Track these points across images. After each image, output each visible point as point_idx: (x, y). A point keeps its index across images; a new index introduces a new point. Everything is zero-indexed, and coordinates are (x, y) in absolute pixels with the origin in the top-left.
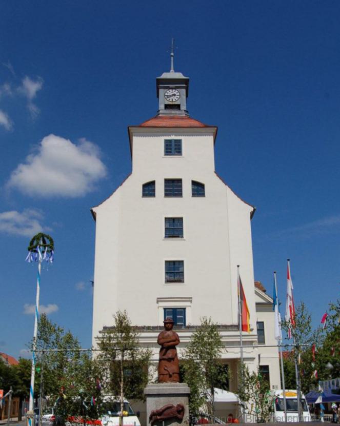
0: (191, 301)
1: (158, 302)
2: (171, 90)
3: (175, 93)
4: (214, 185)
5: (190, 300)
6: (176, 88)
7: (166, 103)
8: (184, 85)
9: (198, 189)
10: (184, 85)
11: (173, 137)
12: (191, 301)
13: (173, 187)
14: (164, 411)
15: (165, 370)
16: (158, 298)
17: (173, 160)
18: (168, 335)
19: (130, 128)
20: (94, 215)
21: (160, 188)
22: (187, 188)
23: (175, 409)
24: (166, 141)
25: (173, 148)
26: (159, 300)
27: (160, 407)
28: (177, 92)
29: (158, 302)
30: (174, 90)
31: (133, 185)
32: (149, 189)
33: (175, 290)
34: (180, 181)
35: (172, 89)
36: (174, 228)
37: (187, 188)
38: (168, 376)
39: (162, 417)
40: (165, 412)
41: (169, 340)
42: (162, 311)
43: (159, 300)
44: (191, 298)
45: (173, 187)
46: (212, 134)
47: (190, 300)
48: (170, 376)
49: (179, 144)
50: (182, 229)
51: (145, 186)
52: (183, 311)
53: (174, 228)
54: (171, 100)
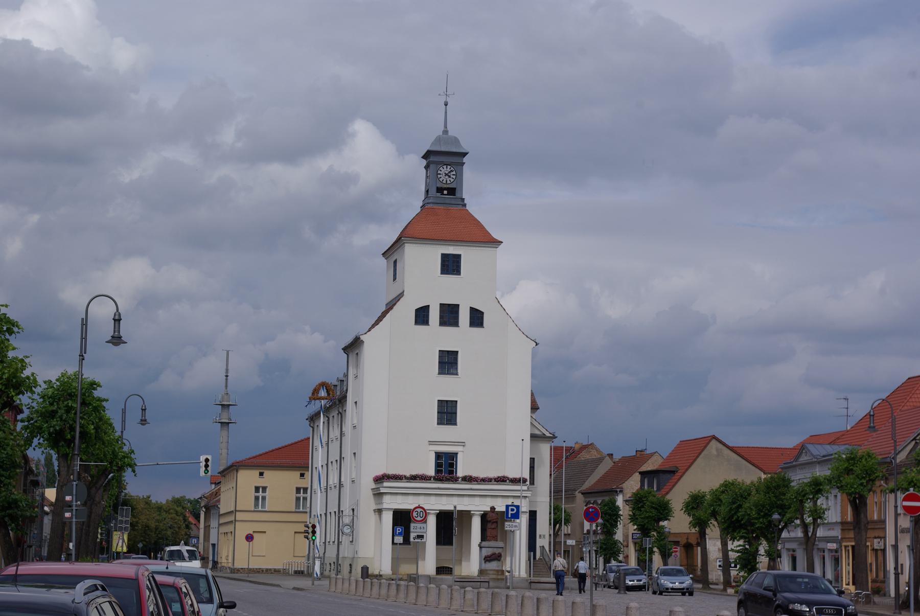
5: (463, 444)
9: (477, 318)
13: (449, 314)
21: (434, 315)
22: (464, 316)
24: (444, 256)
26: (431, 443)
31: (405, 311)
32: (422, 316)
33: (447, 432)
36: (448, 362)
37: (464, 316)
43: (431, 443)
47: (463, 444)
51: (418, 311)
52: (453, 456)
53: (448, 362)
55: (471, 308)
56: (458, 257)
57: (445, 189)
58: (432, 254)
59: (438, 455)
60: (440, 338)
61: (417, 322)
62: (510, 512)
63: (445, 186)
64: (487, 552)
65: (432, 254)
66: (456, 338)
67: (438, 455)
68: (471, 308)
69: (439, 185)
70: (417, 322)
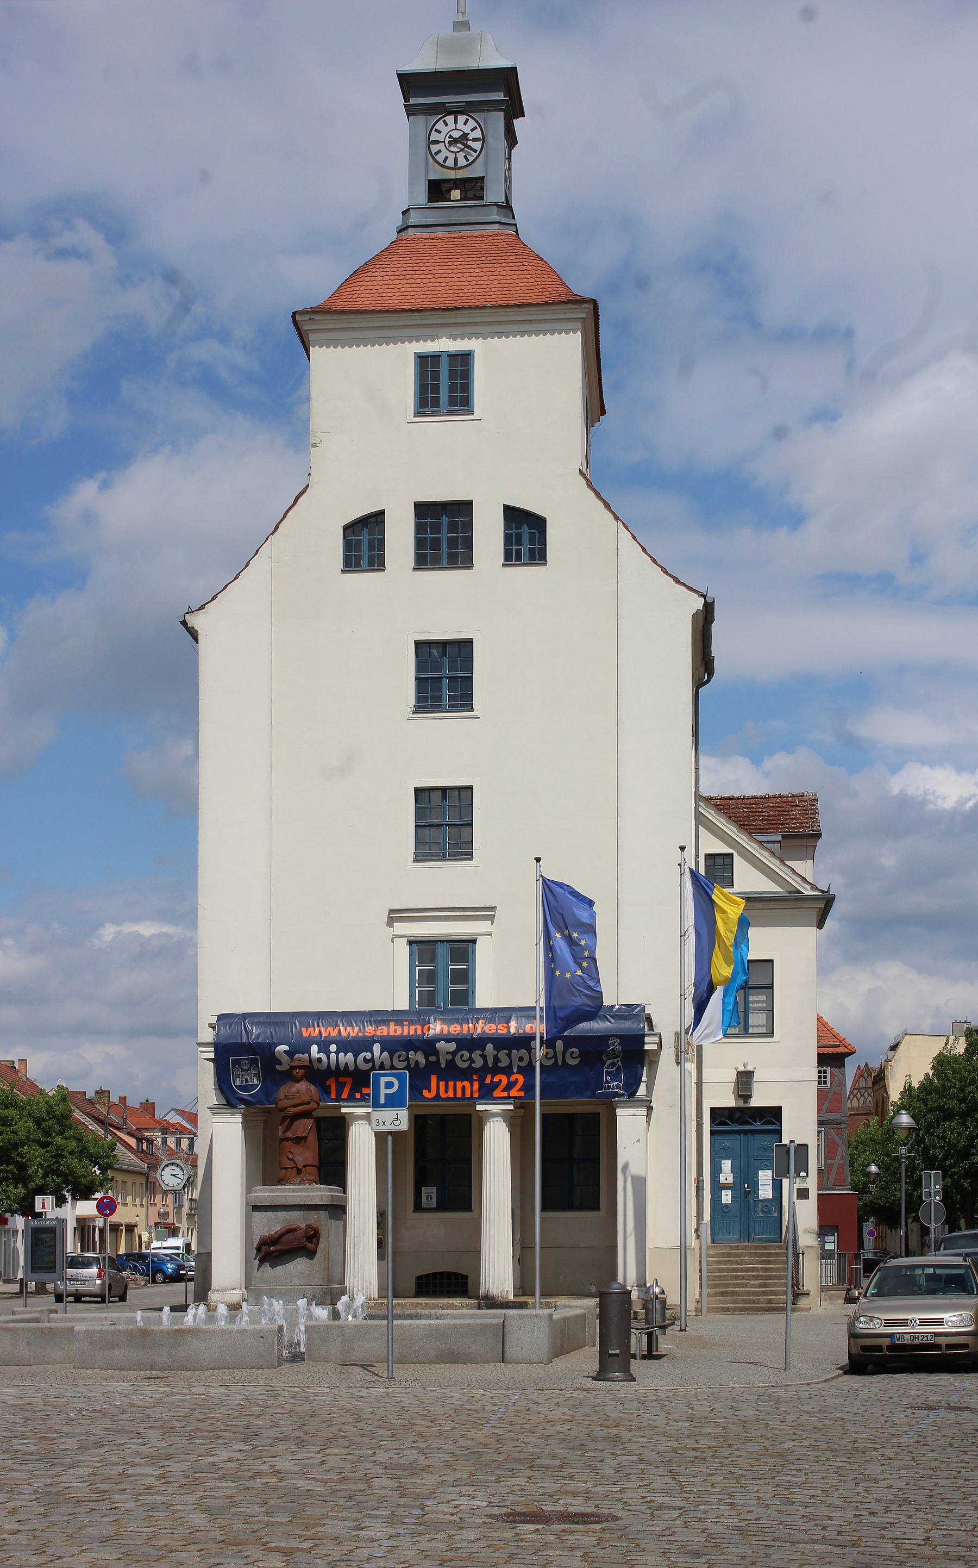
0: (492, 918)
1: (391, 921)
2: (450, 119)
3: (467, 129)
4: (574, 519)
5: (487, 913)
6: (468, 109)
7: (432, 177)
8: (500, 96)
9: (526, 535)
10: (500, 96)
11: (445, 345)
12: (492, 918)
13: (444, 532)
14: (281, 1236)
15: (290, 1159)
16: (392, 911)
17: (444, 429)
18: (298, 1092)
19: (298, 318)
20: (194, 635)
21: (400, 537)
22: (488, 533)
23: (300, 1234)
24: (426, 362)
25: (444, 388)
26: (395, 916)
27: (276, 1229)
28: (472, 124)
29: (391, 921)
30: (462, 118)
32: (363, 542)
33: (444, 882)
34: (464, 508)
35: (456, 112)
36: (444, 675)
37: (488, 533)
38: (295, 1171)
39: (278, 1247)
40: (284, 1239)
41: (297, 1101)
42: (403, 951)
43: (395, 916)
44: (493, 908)
45: (444, 532)
46: (579, 325)
47: (487, 913)
48: (299, 1172)
49: (364, 562)
50: (471, 679)
51: (352, 529)
52: (462, 949)
53: (444, 675)
54: (450, 163)
55: (507, 509)
56: (463, 361)
57: (457, 183)
58: (390, 367)
59: (422, 949)
60: (414, 601)
61: (351, 563)
62: (383, 1091)
63: (452, 175)
64: (270, 1224)
65: (390, 367)
66: (475, 600)
67: (422, 949)
68: (507, 509)
69: (437, 174)
70: (351, 563)
